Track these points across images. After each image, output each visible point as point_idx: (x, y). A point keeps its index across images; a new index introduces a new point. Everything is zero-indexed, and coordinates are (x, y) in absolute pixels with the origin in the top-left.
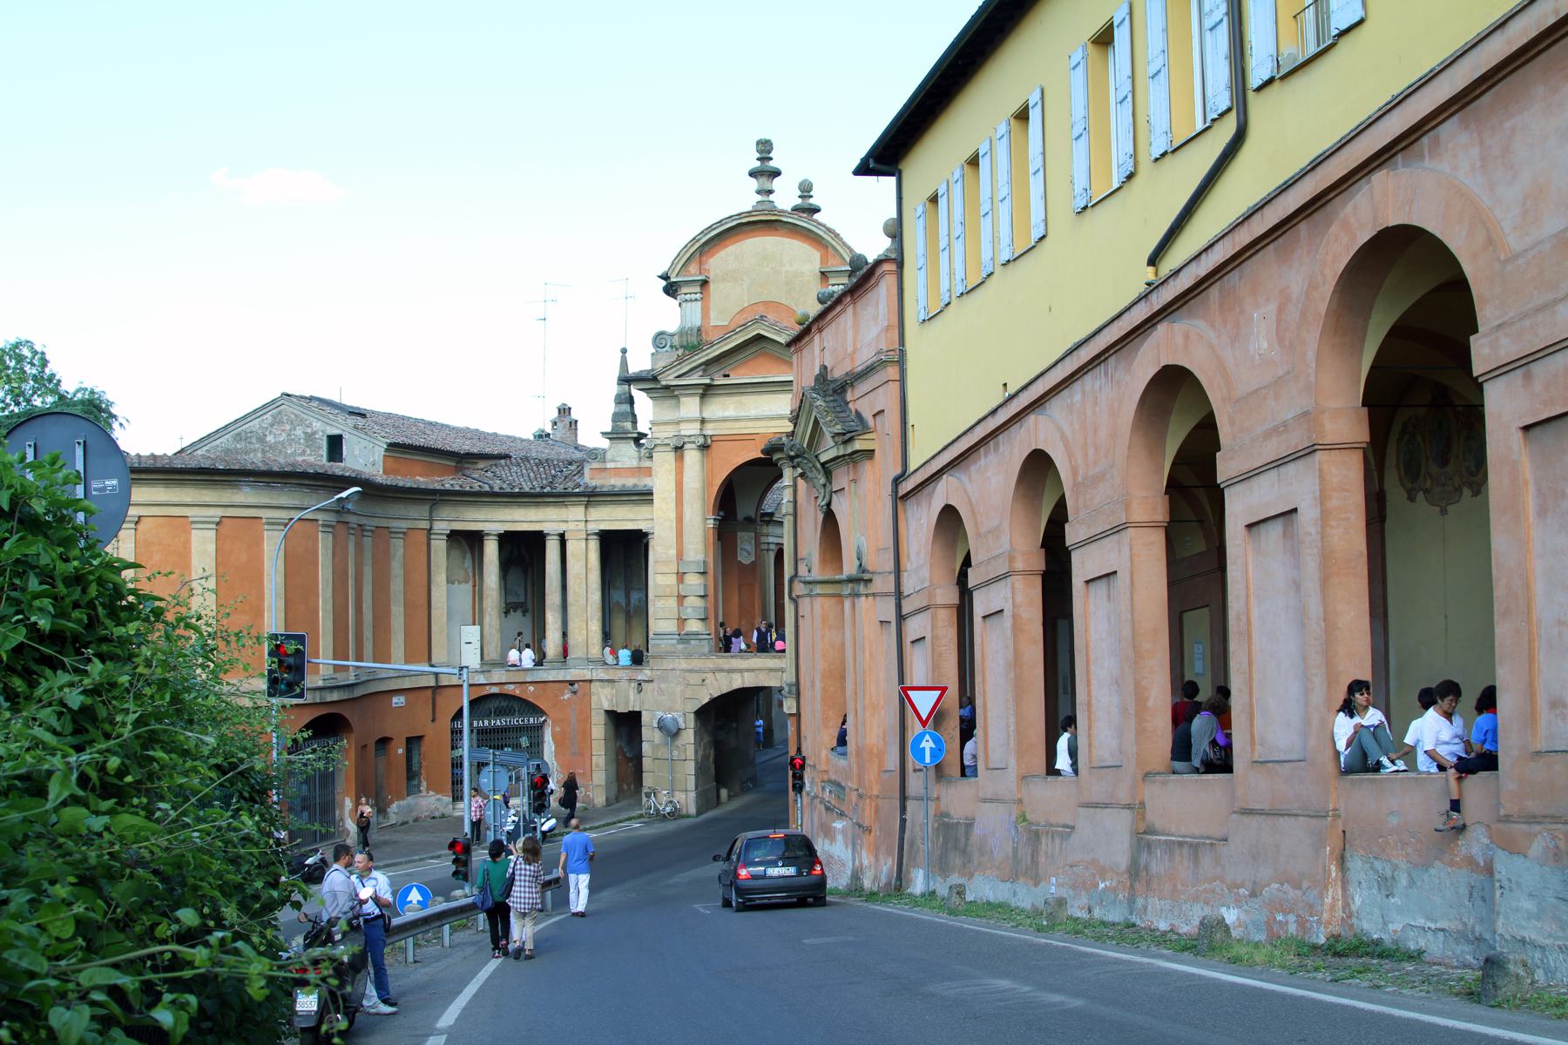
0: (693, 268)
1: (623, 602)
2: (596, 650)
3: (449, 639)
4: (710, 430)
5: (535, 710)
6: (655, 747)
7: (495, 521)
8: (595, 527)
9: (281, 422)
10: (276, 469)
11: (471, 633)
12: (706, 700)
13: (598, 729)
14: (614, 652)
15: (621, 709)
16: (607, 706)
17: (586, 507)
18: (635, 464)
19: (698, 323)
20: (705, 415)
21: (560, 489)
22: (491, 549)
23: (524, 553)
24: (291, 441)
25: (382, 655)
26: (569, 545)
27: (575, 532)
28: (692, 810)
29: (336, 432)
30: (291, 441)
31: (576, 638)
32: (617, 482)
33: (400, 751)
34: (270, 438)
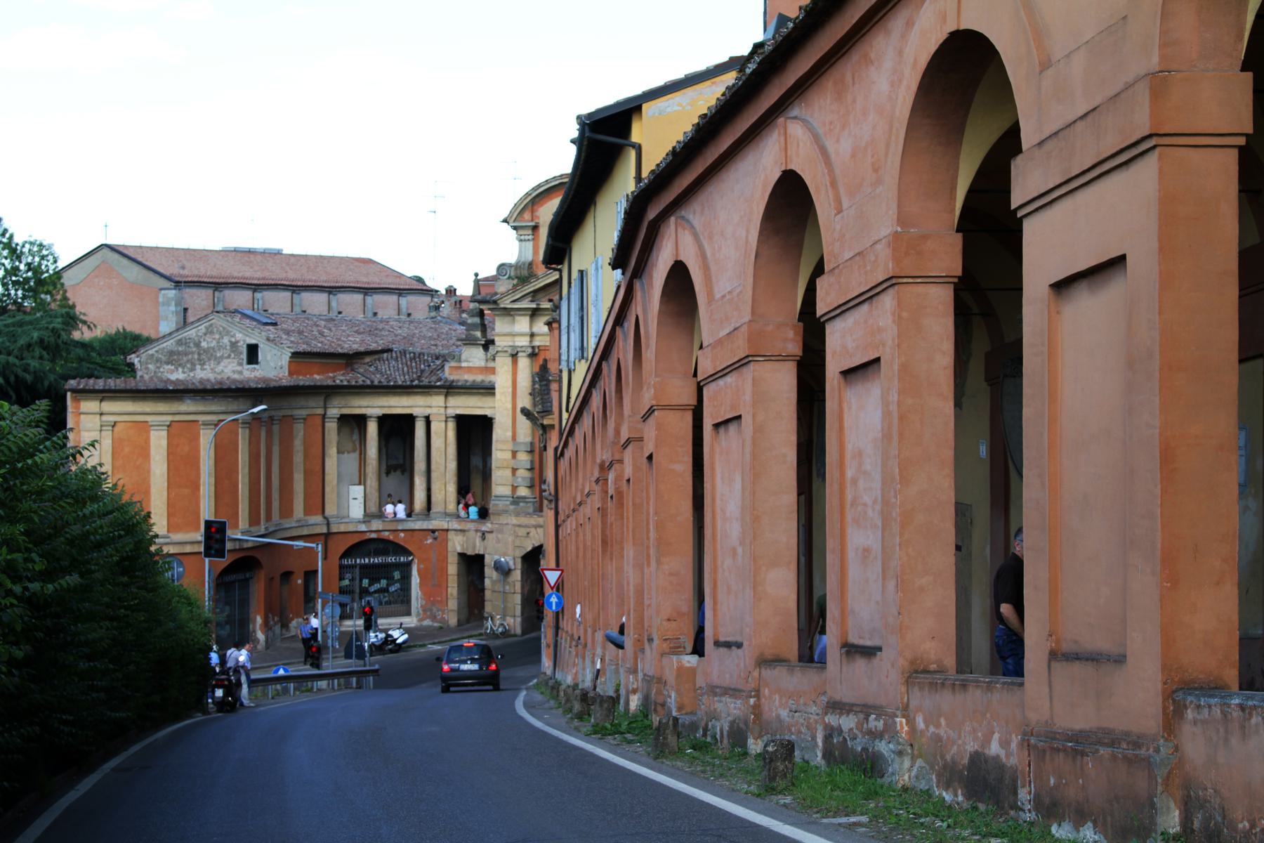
0: (527, 216)
1: (480, 465)
2: (451, 507)
3: (339, 496)
4: (537, 342)
5: (407, 552)
6: (494, 583)
7: (375, 407)
8: (451, 412)
9: (212, 333)
10: (209, 387)
11: (357, 491)
12: (530, 548)
13: (453, 569)
14: (467, 506)
15: (470, 552)
16: (459, 549)
17: (446, 396)
18: (483, 364)
19: (530, 258)
20: (535, 330)
21: (425, 382)
22: (372, 428)
23: (398, 430)
24: (220, 348)
25: (287, 511)
26: (434, 426)
27: (437, 415)
28: (519, 631)
29: (253, 342)
30: (220, 348)
31: (437, 496)
32: (469, 378)
33: (300, 581)
34: (204, 344)
